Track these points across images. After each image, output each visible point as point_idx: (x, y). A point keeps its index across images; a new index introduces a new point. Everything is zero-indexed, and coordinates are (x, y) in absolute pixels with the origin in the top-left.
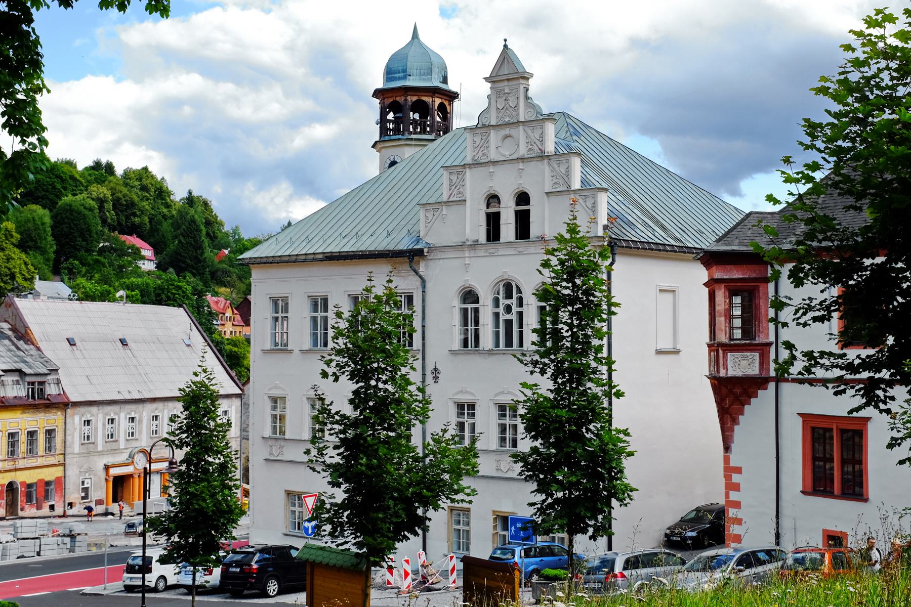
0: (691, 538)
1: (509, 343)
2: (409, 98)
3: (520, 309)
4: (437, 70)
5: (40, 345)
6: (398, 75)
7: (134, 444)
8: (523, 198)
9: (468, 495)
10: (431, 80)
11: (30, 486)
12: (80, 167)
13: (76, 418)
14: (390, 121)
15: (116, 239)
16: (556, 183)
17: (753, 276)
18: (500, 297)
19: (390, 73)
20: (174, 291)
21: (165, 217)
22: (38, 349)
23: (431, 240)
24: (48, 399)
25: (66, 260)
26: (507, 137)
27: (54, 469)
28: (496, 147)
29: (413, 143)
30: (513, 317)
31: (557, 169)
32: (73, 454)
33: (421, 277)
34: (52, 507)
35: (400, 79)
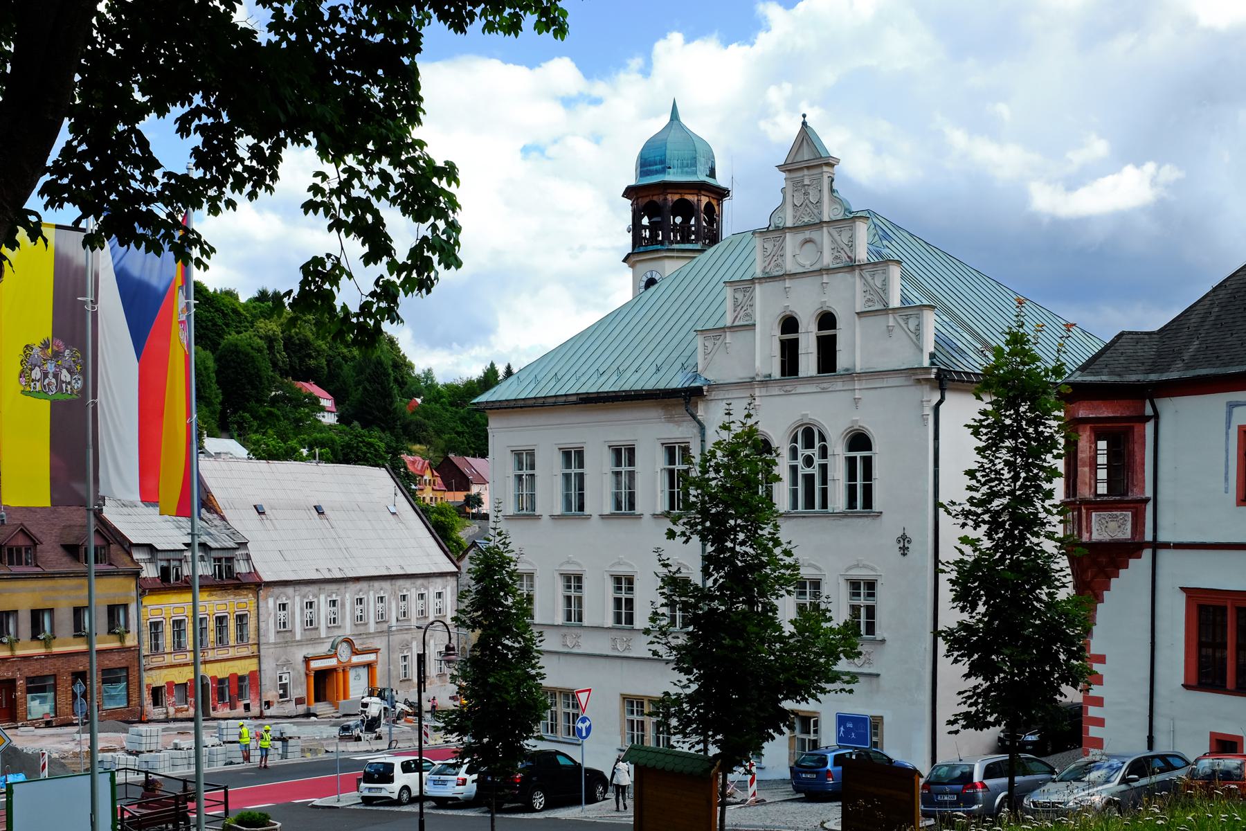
0: (1032, 743)
1: (810, 503)
2: (669, 197)
3: (823, 461)
4: (702, 160)
5: (225, 513)
7: (337, 632)
8: (827, 320)
9: (848, 682)
10: (695, 173)
11: (221, 681)
12: (243, 299)
13: (270, 603)
14: (645, 227)
15: (290, 386)
16: (869, 300)
17: (1127, 413)
18: (799, 446)
19: (646, 164)
20: (364, 449)
21: (344, 358)
22: (223, 518)
23: (713, 375)
24: (237, 579)
25: (235, 412)
26: (807, 241)
27: (247, 661)
28: (794, 254)
29: (675, 254)
30: (815, 470)
31: (871, 282)
32: (268, 644)
33: (699, 422)
34: (247, 707)
35: (657, 172)
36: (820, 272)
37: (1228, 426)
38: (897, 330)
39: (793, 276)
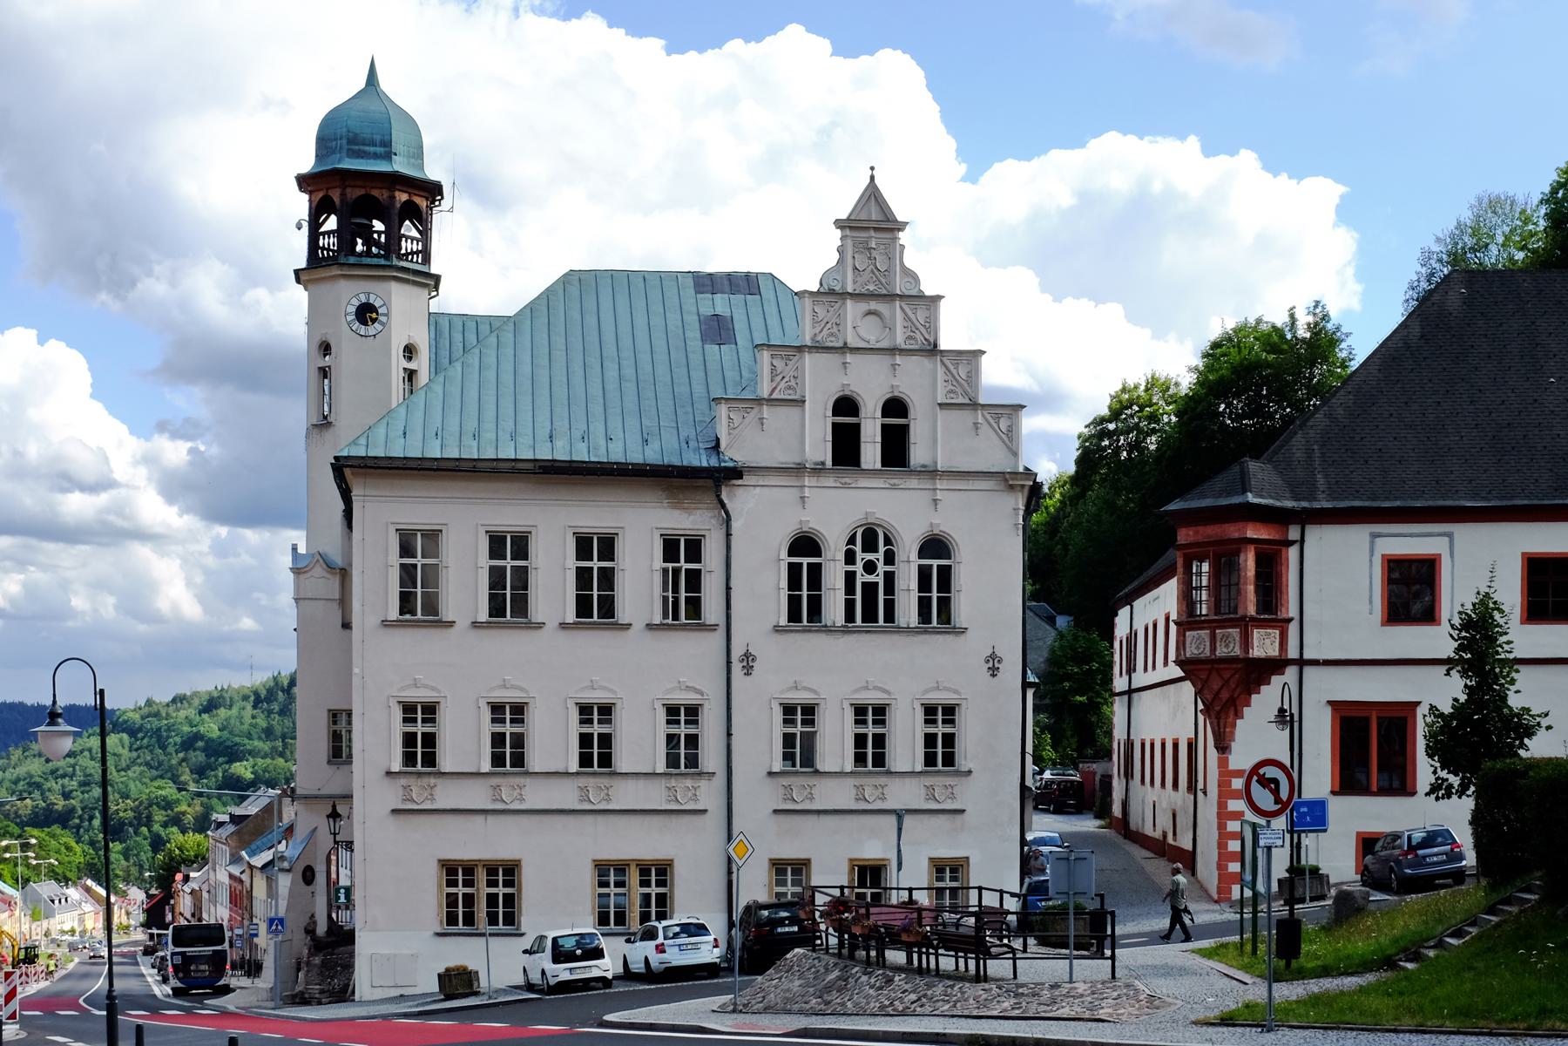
1: (870, 616)
3: (889, 568)
6: (372, 149)
8: (895, 407)
16: (951, 391)
19: (325, 142)
26: (870, 313)
28: (856, 324)
33: (727, 513)
35: (376, 156)
36: (893, 351)
37: (1372, 554)
38: (985, 429)
39: (856, 350)
